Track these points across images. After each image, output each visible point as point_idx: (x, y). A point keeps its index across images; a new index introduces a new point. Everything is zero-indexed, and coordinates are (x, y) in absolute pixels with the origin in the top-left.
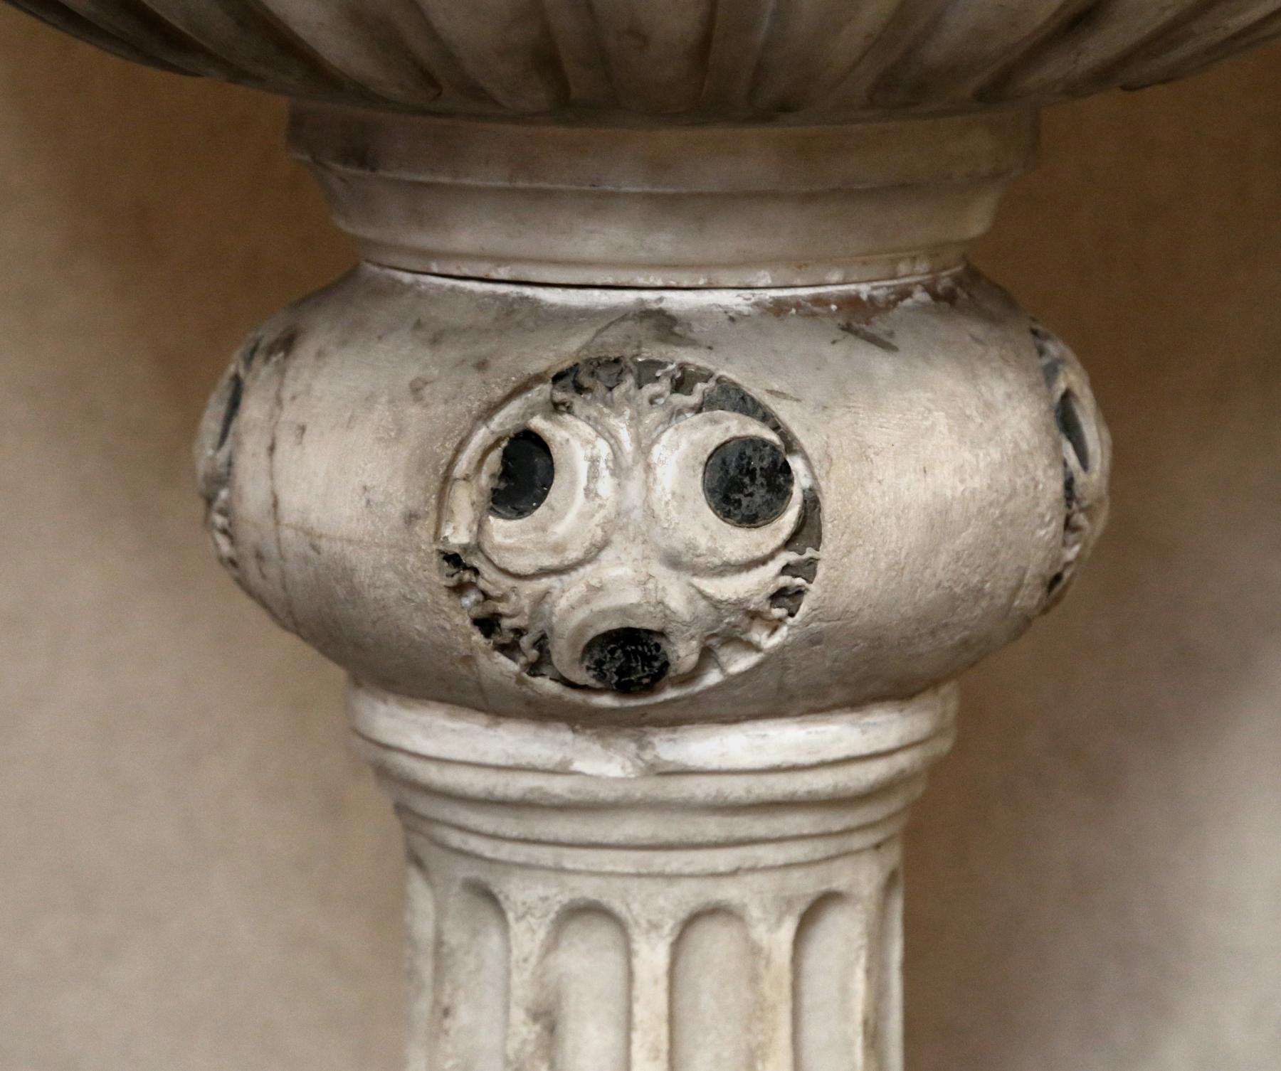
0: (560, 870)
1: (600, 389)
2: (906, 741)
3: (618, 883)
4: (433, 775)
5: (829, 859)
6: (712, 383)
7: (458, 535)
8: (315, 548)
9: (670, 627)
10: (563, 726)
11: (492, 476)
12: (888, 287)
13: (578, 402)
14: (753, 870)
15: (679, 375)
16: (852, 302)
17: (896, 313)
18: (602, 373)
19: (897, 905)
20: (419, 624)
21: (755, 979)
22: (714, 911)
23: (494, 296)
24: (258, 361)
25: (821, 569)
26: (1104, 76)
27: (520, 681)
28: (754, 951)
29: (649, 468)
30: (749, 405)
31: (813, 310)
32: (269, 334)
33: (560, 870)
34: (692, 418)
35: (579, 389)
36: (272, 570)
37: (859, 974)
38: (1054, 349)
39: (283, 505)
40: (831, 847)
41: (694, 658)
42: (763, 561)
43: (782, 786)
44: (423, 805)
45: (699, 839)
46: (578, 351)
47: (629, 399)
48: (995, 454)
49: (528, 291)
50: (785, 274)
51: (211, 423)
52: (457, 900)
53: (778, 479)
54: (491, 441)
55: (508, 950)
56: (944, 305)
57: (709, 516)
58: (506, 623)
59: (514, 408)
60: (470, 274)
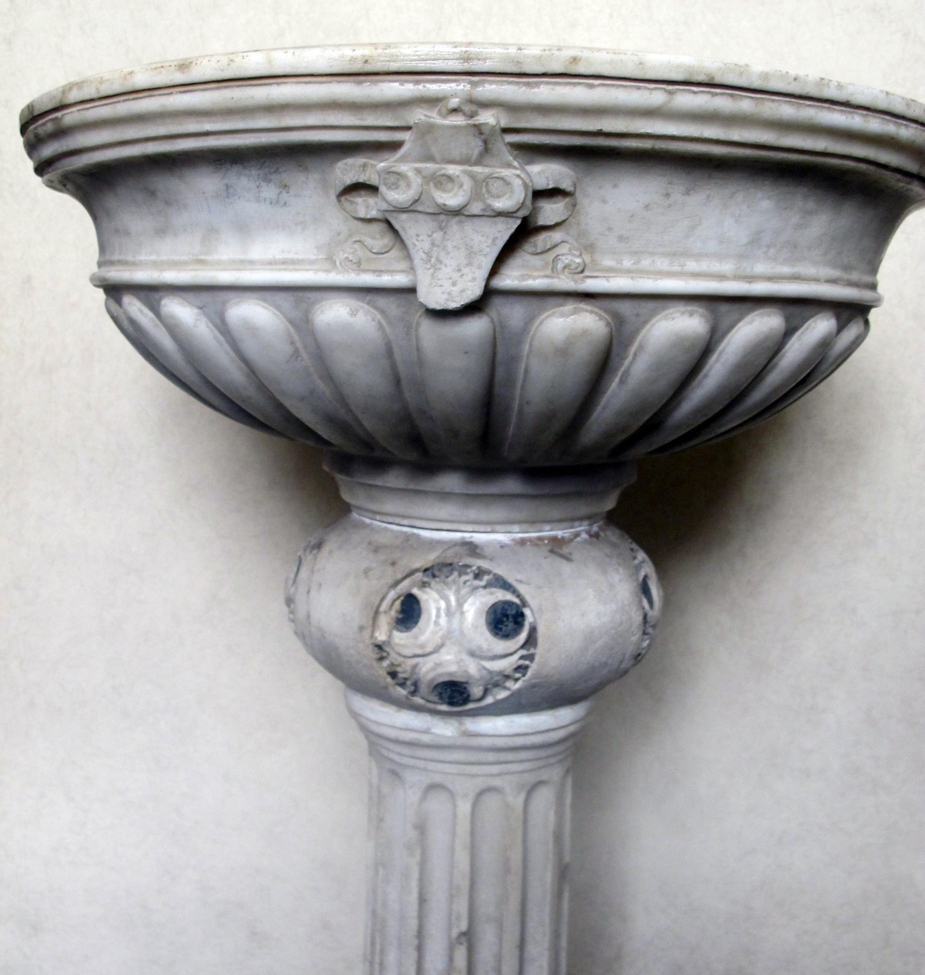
0: (426, 770)
1: (443, 577)
4: (375, 728)
5: (540, 768)
7: (381, 636)
8: (324, 637)
9: (470, 681)
11: (397, 612)
12: (570, 532)
13: (433, 583)
15: (477, 572)
16: (554, 540)
17: (573, 544)
20: (365, 673)
23: (402, 532)
24: (308, 551)
25: (537, 658)
29: (462, 613)
30: (507, 586)
33: (426, 770)
34: (482, 591)
35: (434, 576)
40: (542, 763)
42: (511, 654)
43: (520, 741)
46: (434, 560)
47: (454, 581)
48: (614, 607)
49: (416, 531)
50: (525, 527)
53: (518, 618)
56: (594, 539)
58: (401, 675)
59: (406, 583)
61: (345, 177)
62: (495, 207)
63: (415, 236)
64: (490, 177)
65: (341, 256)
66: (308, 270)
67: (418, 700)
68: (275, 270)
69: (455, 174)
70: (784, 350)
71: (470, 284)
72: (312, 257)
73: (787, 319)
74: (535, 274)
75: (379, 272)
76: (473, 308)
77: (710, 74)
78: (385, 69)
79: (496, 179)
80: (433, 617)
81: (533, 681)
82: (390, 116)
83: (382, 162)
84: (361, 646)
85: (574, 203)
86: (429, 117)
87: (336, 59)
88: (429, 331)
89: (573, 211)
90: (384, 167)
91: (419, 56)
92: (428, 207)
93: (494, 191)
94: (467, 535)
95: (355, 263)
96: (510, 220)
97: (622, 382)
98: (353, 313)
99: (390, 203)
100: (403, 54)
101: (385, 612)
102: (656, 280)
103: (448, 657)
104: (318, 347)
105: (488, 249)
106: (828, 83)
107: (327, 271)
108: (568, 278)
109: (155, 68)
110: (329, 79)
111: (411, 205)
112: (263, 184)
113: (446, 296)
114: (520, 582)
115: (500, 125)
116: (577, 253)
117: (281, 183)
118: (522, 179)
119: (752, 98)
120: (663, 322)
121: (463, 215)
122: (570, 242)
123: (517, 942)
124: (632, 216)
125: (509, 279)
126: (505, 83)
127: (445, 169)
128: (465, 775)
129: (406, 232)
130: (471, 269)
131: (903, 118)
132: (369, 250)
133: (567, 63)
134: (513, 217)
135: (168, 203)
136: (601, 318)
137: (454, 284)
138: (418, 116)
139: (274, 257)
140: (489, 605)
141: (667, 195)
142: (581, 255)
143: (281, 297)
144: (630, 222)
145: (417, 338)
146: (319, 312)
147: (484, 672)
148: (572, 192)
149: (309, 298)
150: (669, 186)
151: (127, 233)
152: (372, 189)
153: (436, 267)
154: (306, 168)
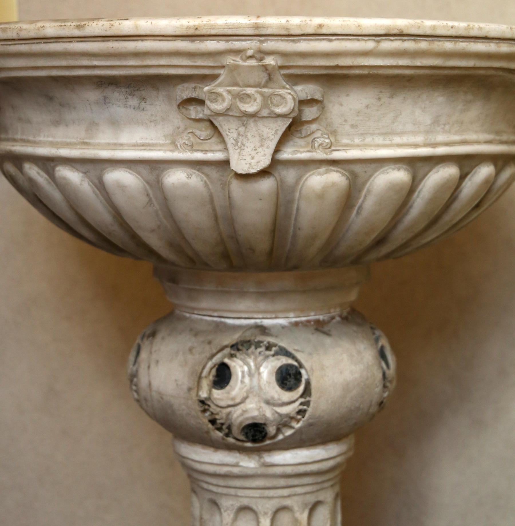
0: (237, 496)
1: (244, 350)
4: (198, 466)
5: (318, 491)
7: (204, 395)
8: (162, 398)
9: (267, 422)
10: (236, 451)
11: (213, 376)
13: (238, 354)
14: (295, 495)
15: (267, 345)
18: (245, 345)
19: (339, 503)
20: (193, 422)
22: (284, 508)
23: (213, 321)
24: (145, 340)
25: (312, 404)
26: (388, 256)
29: (259, 374)
31: (306, 324)
33: (237, 496)
34: (272, 359)
35: (238, 350)
38: (378, 332)
42: (294, 402)
44: (196, 475)
45: (278, 486)
47: (253, 353)
48: (362, 367)
49: (223, 320)
51: (132, 358)
52: (206, 505)
53: (298, 376)
54: (213, 365)
55: (222, 521)
57: (278, 388)
58: (219, 422)
61: (183, 94)
62: (276, 112)
63: (228, 130)
64: (272, 94)
65: (180, 142)
66: (159, 150)
67: (231, 440)
68: (138, 150)
69: (251, 93)
71: (263, 158)
72: (161, 142)
73: (461, 168)
74: (301, 150)
75: (205, 151)
76: (264, 173)
77: (400, 29)
78: (208, 33)
79: (276, 95)
81: (311, 421)
82: (211, 60)
83: (207, 86)
84: (190, 402)
85: (323, 107)
87: (178, 27)
88: (236, 187)
89: (323, 112)
90: (208, 89)
91: (228, 26)
92: (236, 112)
94: (258, 321)
95: (190, 146)
96: (285, 119)
97: (358, 213)
98: (189, 177)
99: (212, 110)
100: (218, 25)
102: (376, 150)
104: (165, 199)
105: (273, 137)
106: (473, 27)
108: (322, 152)
109: (60, 26)
110: (174, 38)
111: (225, 111)
112: (129, 97)
113: (248, 166)
115: (278, 64)
116: (326, 136)
117: (141, 96)
118: (292, 95)
119: (426, 40)
120: (382, 175)
121: (257, 117)
122: (322, 130)
124: (359, 112)
125: (286, 154)
126: (280, 41)
127: (245, 90)
128: (264, 498)
129: (222, 127)
130: (263, 149)
132: (198, 138)
133: (316, 28)
134: (287, 117)
135: (62, 105)
136: (343, 175)
138: (229, 60)
139: (136, 141)
140: (277, 367)
141: (379, 99)
142: (329, 137)
143: (141, 168)
144: (358, 116)
146: (167, 176)
147: (276, 415)
148: (322, 100)
149: (160, 168)
150: (380, 93)
151: (29, 122)
152: (201, 102)
153: (241, 148)
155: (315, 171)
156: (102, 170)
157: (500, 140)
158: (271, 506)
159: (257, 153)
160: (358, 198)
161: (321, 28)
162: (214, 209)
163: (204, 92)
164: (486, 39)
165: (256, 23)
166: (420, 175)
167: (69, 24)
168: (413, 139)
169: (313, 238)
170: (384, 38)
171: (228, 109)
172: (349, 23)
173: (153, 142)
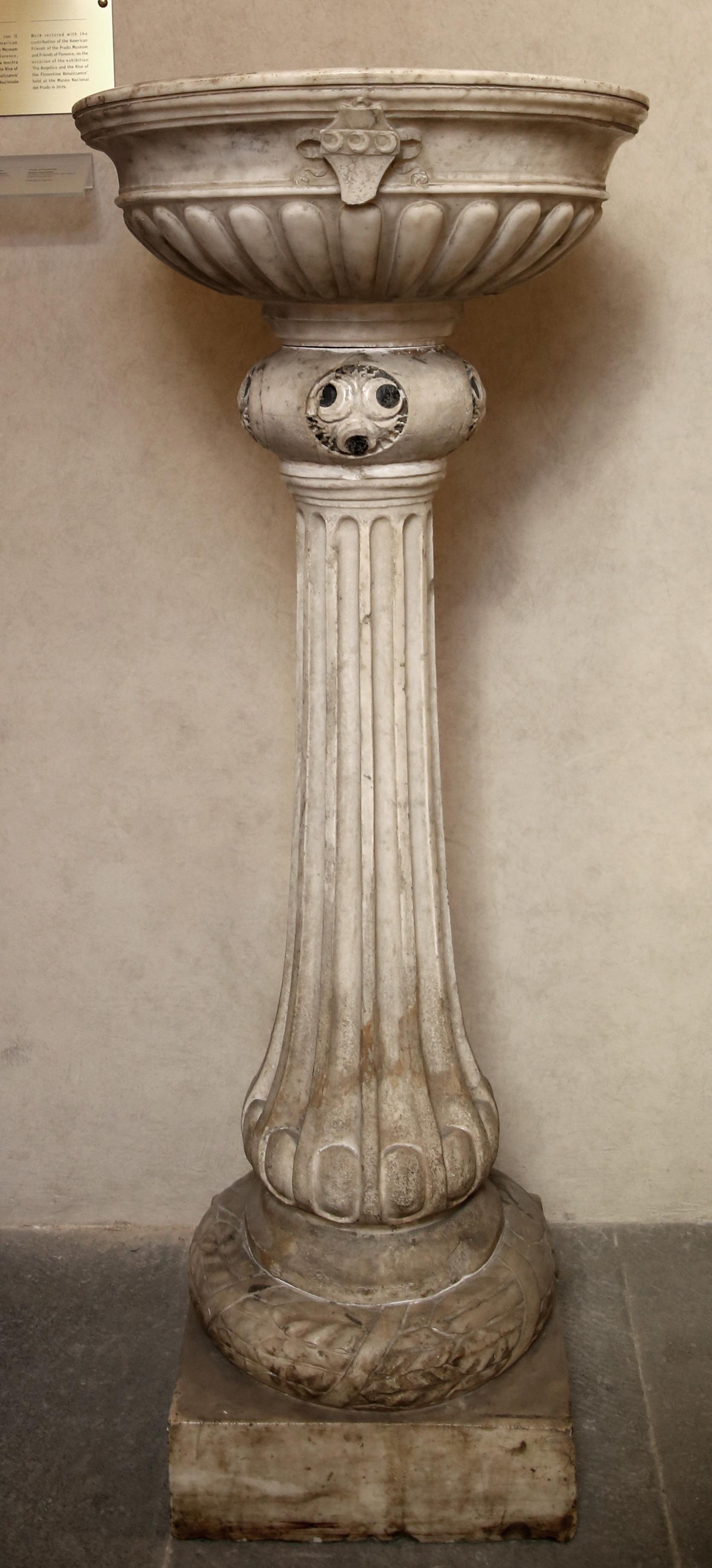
2: (432, 472)
3: (356, 511)
5: (413, 504)
6: (378, 371)
7: (311, 413)
9: (369, 435)
10: (340, 466)
11: (320, 397)
13: (343, 376)
14: (392, 506)
16: (415, 351)
17: (426, 354)
18: (349, 369)
19: (432, 520)
20: (301, 437)
21: (393, 537)
23: (319, 351)
25: (408, 420)
27: (329, 452)
28: (392, 529)
29: (362, 392)
32: (257, 366)
35: (343, 373)
36: (261, 427)
37: (421, 537)
38: (469, 366)
39: (263, 408)
41: (375, 444)
42: (392, 417)
47: (356, 375)
48: (453, 391)
49: (328, 349)
50: (396, 344)
51: (243, 387)
52: (311, 519)
53: (396, 395)
54: (320, 387)
58: (325, 435)
60: (312, 345)
65: (298, 179)
66: (280, 186)
67: (336, 453)
68: (261, 187)
70: (542, 224)
73: (542, 206)
75: (320, 186)
76: (370, 204)
80: (345, 396)
83: (322, 129)
86: (348, 106)
88: (346, 217)
93: (380, 142)
96: (389, 157)
98: (305, 209)
101: (313, 398)
103: (355, 420)
104: (284, 230)
107: (291, 187)
112: (255, 141)
113: (356, 197)
114: (396, 374)
116: (424, 173)
123: (403, 623)
125: (389, 188)
131: (597, 93)
135: (193, 152)
136: (438, 207)
137: (361, 191)
138: (343, 106)
140: (378, 387)
141: (470, 141)
144: (451, 155)
145: (340, 222)
151: (161, 169)
152: (317, 143)
154: (279, 133)
155: (413, 203)
156: (229, 208)
157: (578, 183)
158: (371, 515)
159: (365, 187)
160: (451, 229)
161: (421, 78)
162: (326, 239)
163: (320, 134)
164: (562, 90)
165: (365, 74)
166: (505, 209)
167: (204, 79)
168: (498, 177)
169: (411, 265)
170: (473, 87)
171: (340, 149)
172: (443, 73)
173: (274, 179)
